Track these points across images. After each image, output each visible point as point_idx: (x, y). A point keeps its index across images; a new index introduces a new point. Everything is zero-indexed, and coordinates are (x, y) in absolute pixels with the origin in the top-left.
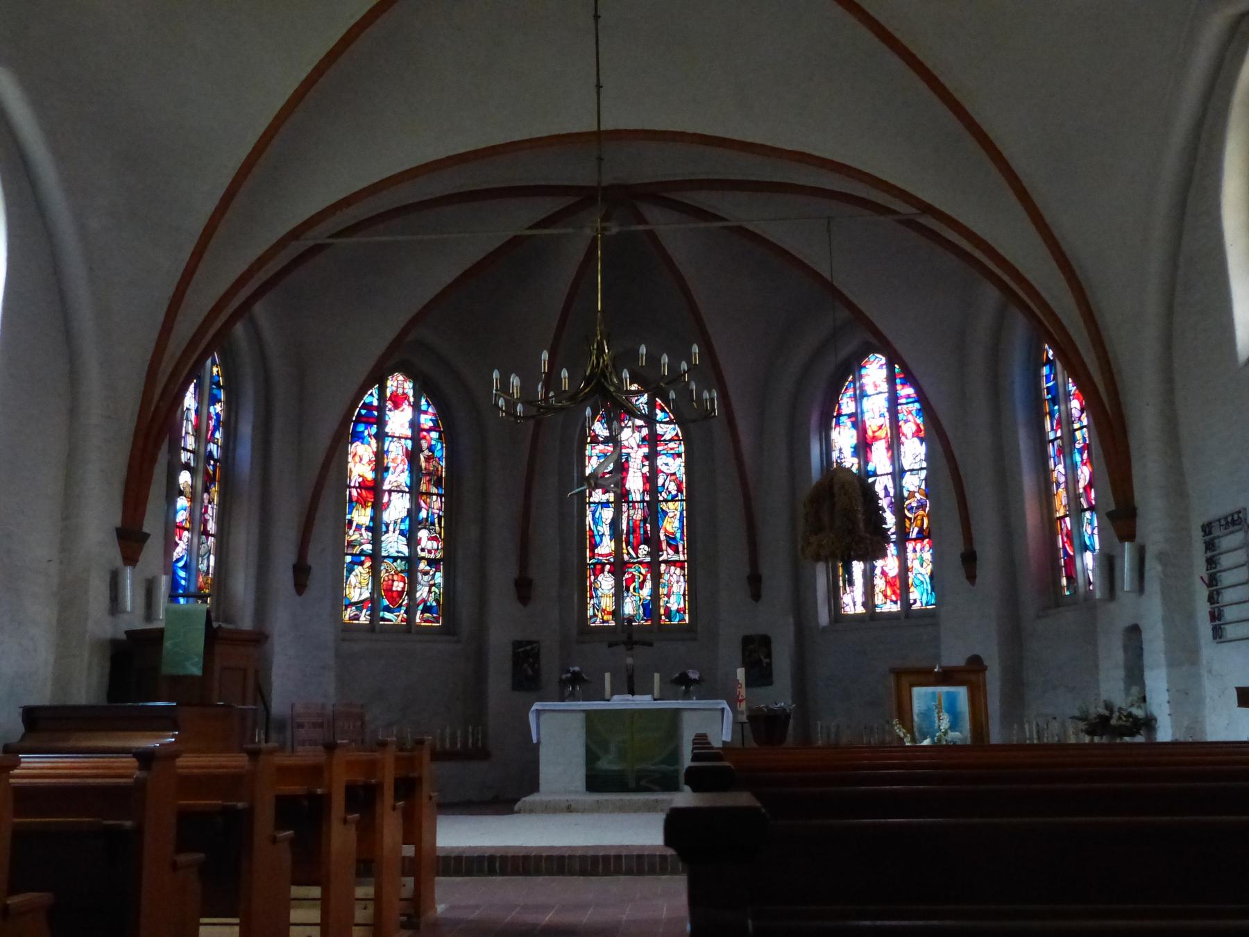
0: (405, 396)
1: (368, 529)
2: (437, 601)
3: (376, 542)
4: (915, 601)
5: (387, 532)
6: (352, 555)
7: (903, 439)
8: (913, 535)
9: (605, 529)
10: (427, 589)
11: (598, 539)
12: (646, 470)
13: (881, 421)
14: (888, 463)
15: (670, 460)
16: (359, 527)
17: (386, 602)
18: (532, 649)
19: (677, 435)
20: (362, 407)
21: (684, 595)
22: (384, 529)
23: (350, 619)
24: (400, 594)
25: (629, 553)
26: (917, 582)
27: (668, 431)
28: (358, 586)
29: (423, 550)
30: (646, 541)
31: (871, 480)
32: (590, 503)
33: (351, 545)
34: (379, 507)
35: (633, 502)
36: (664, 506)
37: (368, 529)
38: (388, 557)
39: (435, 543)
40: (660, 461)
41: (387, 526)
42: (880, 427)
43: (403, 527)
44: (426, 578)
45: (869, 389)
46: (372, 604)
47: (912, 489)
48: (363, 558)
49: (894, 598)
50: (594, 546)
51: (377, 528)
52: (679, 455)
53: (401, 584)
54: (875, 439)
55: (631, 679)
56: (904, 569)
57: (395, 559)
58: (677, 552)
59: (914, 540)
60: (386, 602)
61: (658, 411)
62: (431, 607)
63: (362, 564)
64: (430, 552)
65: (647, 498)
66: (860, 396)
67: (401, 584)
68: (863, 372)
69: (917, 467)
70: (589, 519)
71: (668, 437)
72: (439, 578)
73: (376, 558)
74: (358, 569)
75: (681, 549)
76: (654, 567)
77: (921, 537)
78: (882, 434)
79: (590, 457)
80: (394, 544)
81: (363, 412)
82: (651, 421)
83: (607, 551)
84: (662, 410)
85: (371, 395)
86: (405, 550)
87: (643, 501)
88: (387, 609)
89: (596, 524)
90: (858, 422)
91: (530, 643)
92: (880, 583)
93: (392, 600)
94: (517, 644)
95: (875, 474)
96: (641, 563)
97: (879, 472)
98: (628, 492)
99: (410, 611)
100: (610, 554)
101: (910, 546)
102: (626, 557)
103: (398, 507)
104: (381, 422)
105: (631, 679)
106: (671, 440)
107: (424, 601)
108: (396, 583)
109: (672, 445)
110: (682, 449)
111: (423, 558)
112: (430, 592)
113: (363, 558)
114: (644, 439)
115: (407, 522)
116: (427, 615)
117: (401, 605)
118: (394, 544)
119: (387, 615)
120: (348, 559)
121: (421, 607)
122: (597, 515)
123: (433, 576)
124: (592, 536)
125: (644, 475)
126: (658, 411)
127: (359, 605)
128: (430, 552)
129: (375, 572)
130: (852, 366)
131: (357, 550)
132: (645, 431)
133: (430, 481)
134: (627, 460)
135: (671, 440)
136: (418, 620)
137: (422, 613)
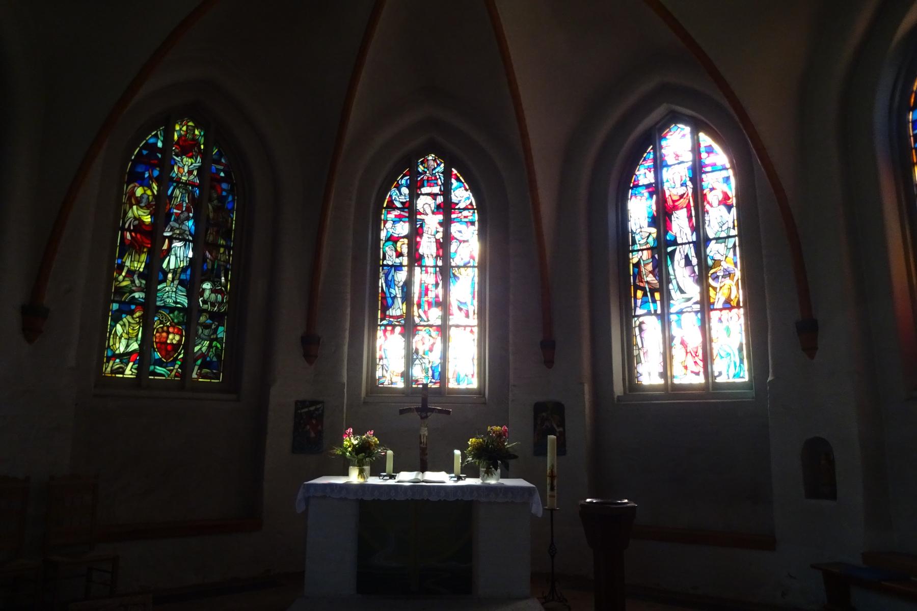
0: (196, 143)
1: (141, 275)
2: (218, 355)
3: (150, 291)
4: (720, 374)
5: (165, 280)
6: (119, 302)
7: (707, 207)
8: (719, 305)
9: (397, 292)
10: (207, 343)
11: (390, 301)
12: (440, 236)
13: (682, 190)
14: (688, 230)
15: (463, 227)
16: (131, 273)
17: (158, 355)
18: (317, 410)
19: (471, 204)
20: (144, 147)
21: (740, 350)
22: (161, 277)
23: (112, 372)
24: (175, 347)
25: (420, 316)
26: (723, 354)
27: (462, 195)
28: (124, 338)
29: (205, 302)
30: (438, 304)
31: (670, 249)
32: (383, 265)
33: (120, 291)
34: (157, 255)
35: (426, 267)
36: (456, 271)
37: (141, 275)
38: (165, 307)
39: (219, 297)
40: (455, 228)
41: (165, 274)
42: (681, 197)
43: (183, 277)
44: (206, 332)
45: (670, 159)
46: (143, 357)
47: (717, 257)
48: (133, 307)
49: (696, 369)
50: (386, 307)
51: (154, 274)
52: (473, 223)
53: (177, 338)
54: (676, 208)
55: (423, 451)
56: (707, 341)
57: (172, 310)
58: (467, 316)
59: (721, 310)
60: (158, 355)
61: (453, 181)
62: (211, 362)
63: (131, 313)
64: (213, 305)
65: (440, 263)
66: (659, 165)
67: (177, 338)
68: (664, 143)
69: (724, 235)
70: (382, 281)
71: (462, 205)
72: (221, 332)
73: (149, 309)
74: (127, 319)
75: (471, 313)
76: (443, 329)
77: (728, 305)
78: (683, 202)
79: (386, 222)
80: (172, 294)
81: (145, 152)
82: (446, 191)
83: (398, 313)
84: (458, 179)
85: (156, 136)
86: (184, 301)
87: (436, 266)
88: (159, 363)
89: (388, 286)
90: (656, 189)
91: (314, 403)
92: (678, 352)
93: (167, 354)
94: (300, 404)
95: (674, 243)
96: (431, 326)
97: (679, 241)
98: (421, 257)
99: (186, 366)
100: (401, 316)
101: (714, 315)
102: (417, 320)
103: (180, 255)
104: (166, 165)
105: (423, 451)
106: (465, 209)
107: (203, 356)
108: (171, 336)
109: (466, 213)
110: (476, 217)
111: (205, 311)
112: (210, 346)
113: (133, 307)
114: (438, 207)
115: (189, 272)
116: (205, 370)
117: (176, 359)
118: (172, 294)
119: (159, 369)
120: (115, 306)
121: (199, 362)
122: (390, 278)
123: (216, 330)
124: (384, 298)
125: (437, 241)
126: (453, 181)
127: (125, 357)
128: (213, 305)
129: (146, 324)
130: (652, 138)
131: (126, 298)
132: (440, 199)
133: (218, 232)
134: (421, 225)
135: (465, 209)
136: (194, 376)
137: (201, 368)
